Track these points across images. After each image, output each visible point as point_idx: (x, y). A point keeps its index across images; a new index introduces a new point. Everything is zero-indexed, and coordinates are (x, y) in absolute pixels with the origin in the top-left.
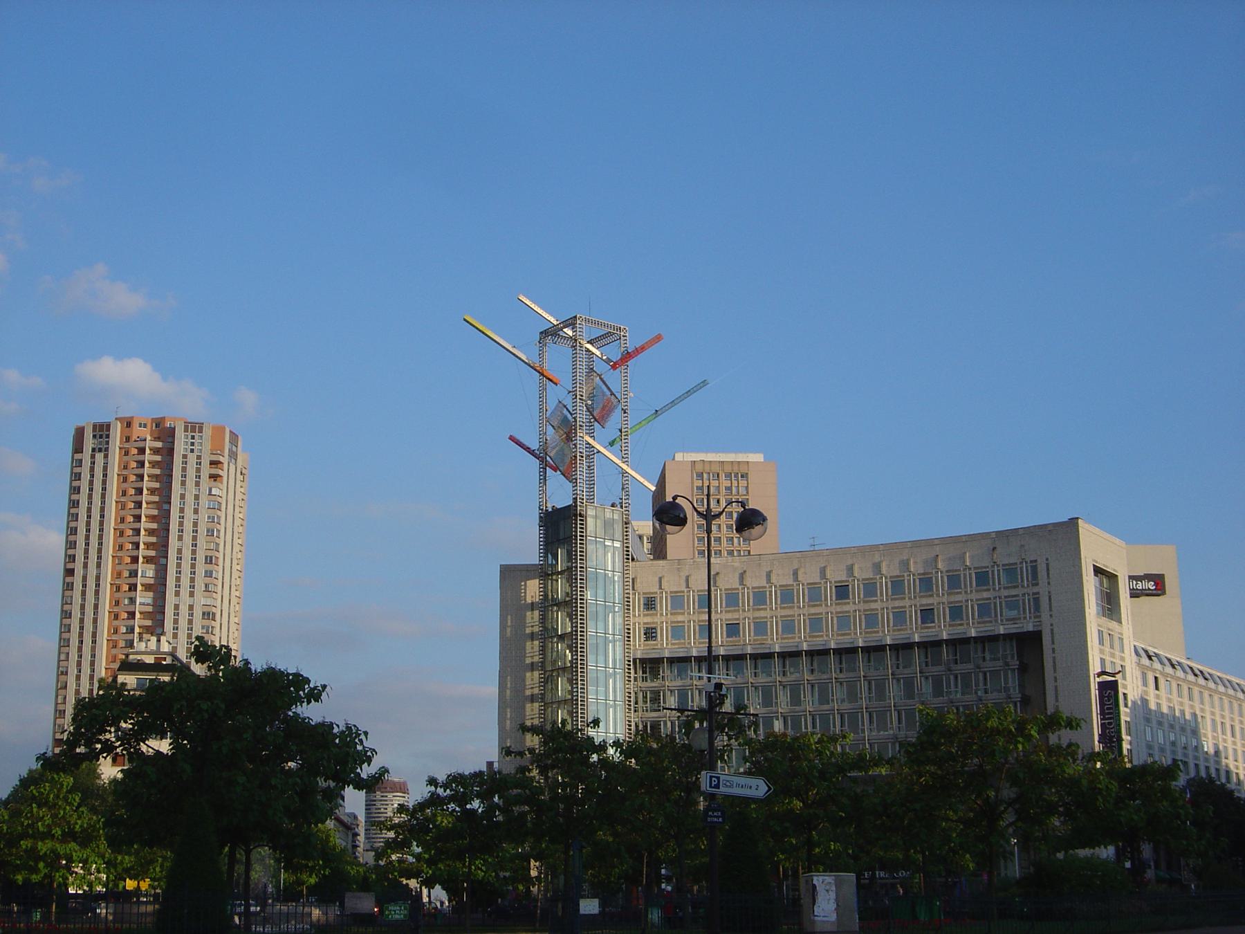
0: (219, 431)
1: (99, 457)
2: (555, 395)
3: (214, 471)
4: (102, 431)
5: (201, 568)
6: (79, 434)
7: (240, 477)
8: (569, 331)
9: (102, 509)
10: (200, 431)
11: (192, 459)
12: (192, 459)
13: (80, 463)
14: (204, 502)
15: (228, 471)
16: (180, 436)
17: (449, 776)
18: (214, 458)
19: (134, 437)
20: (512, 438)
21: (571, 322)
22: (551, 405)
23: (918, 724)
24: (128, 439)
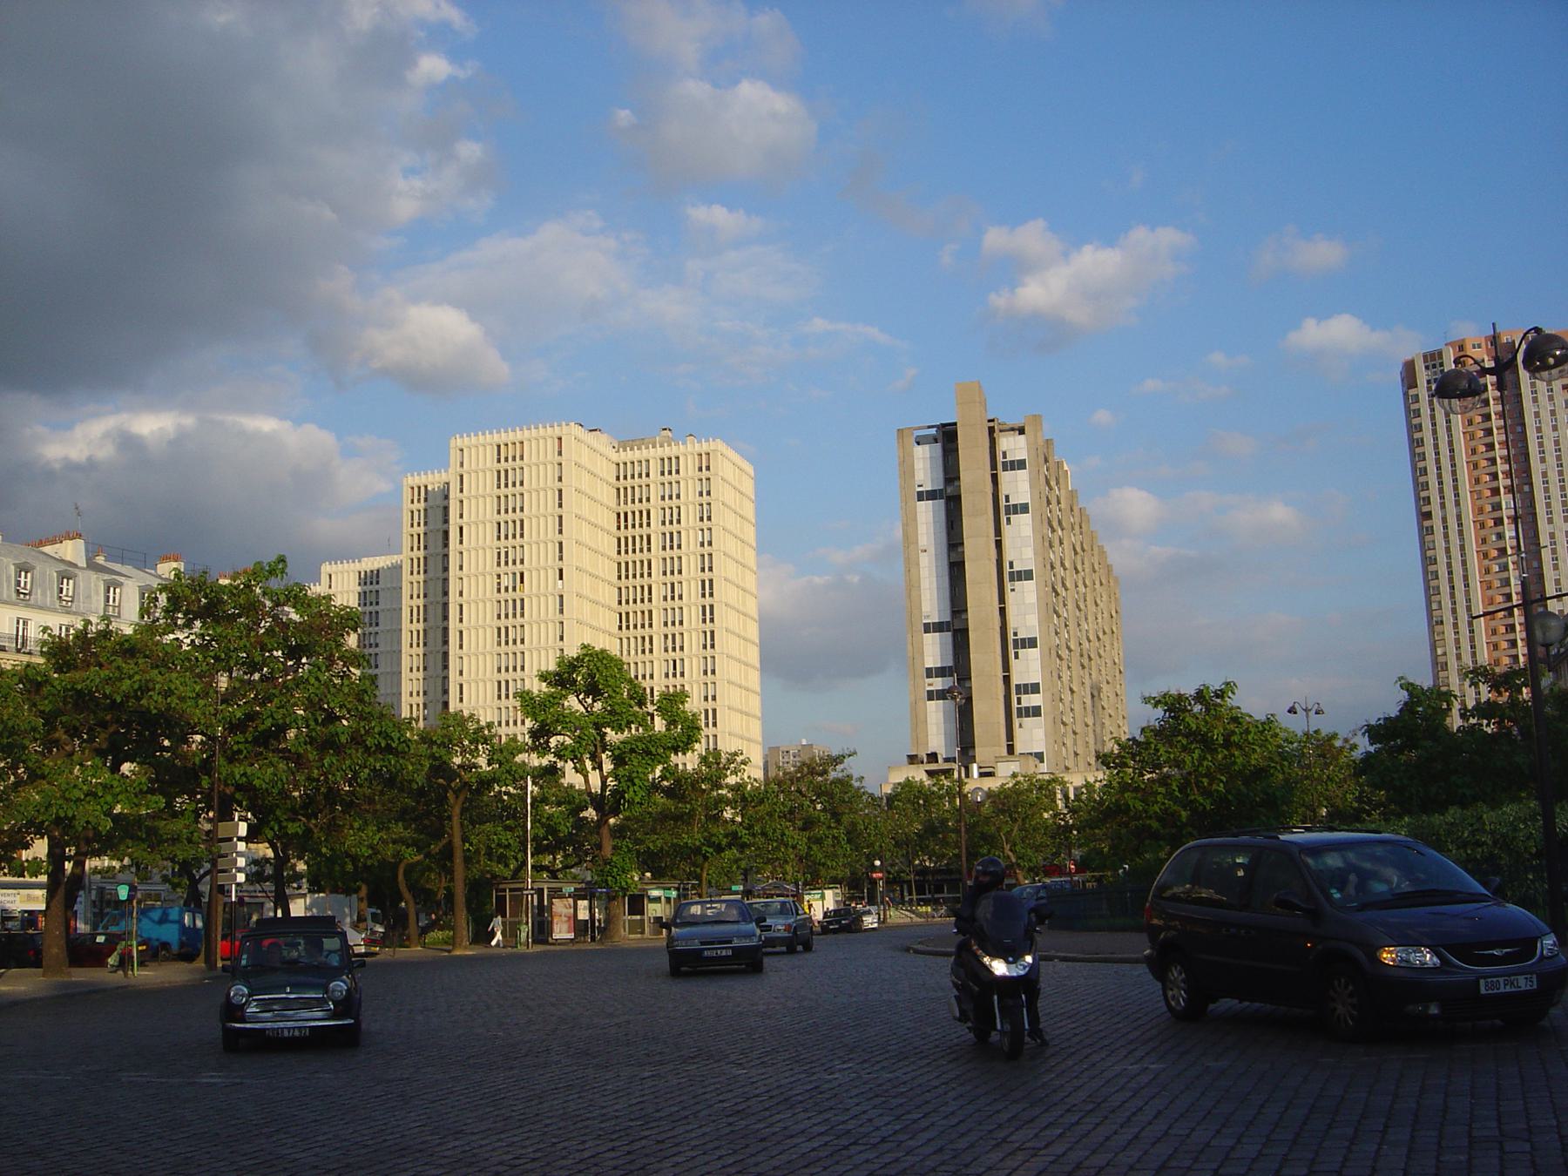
9: (1451, 443)
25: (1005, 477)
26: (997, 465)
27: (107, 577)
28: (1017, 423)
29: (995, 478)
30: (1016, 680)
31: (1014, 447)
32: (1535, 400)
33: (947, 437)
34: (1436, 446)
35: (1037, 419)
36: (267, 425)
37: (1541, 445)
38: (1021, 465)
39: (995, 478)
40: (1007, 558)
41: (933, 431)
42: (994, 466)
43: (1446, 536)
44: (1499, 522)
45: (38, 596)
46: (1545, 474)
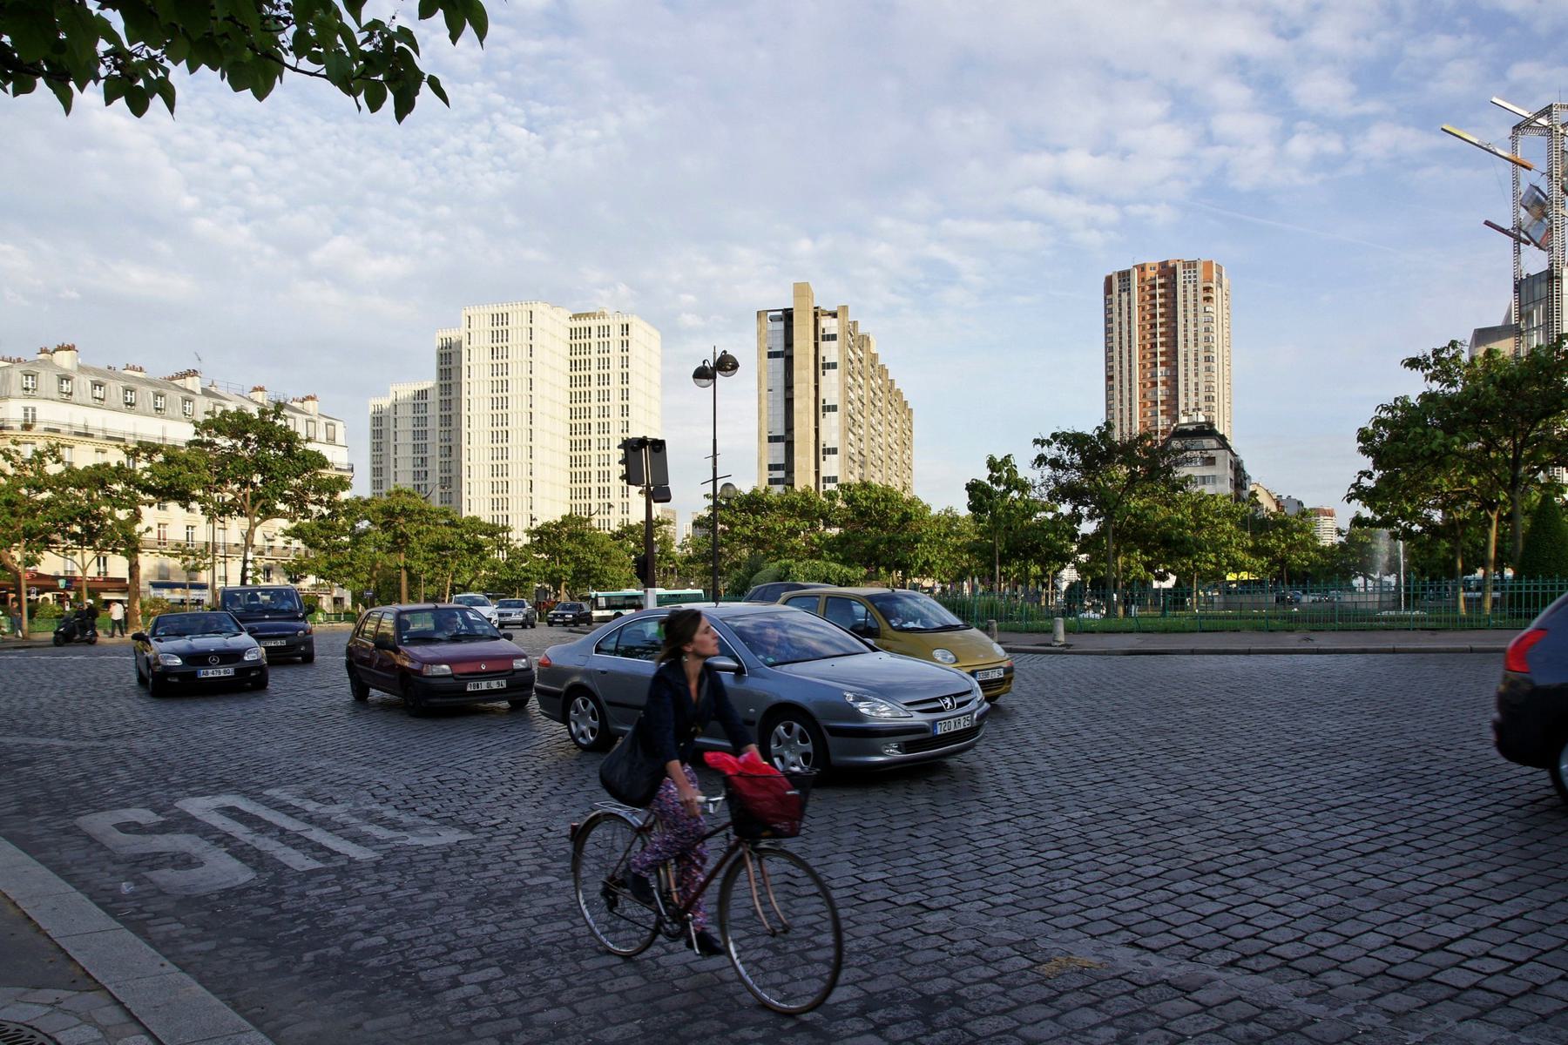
0: (1208, 265)
1: (1124, 295)
2: (1526, 178)
3: (1206, 295)
4: (1125, 276)
5: (1202, 366)
6: (1109, 280)
7: (1225, 311)
8: (1543, 121)
9: (1129, 332)
10: (1195, 266)
11: (1190, 287)
12: (1190, 287)
13: (1111, 301)
14: (1201, 317)
15: (1216, 293)
16: (1180, 270)
17: (946, 511)
18: (1206, 285)
19: (1148, 278)
20: (1487, 223)
21: (1547, 112)
22: (1524, 188)
23: (1050, 515)
24: (1143, 280)
25: (823, 345)
26: (820, 337)
27: (215, 400)
28: (833, 309)
29: (816, 345)
30: (823, 474)
31: (830, 325)
32: (1186, 395)
33: (788, 316)
34: (1120, 333)
35: (845, 308)
36: (436, 700)
37: (1186, 336)
38: (834, 337)
39: (816, 345)
40: (821, 397)
41: (780, 313)
42: (816, 338)
43: (1121, 391)
44: (1155, 384)
45: (169, 411)
46: (1186, 355)
